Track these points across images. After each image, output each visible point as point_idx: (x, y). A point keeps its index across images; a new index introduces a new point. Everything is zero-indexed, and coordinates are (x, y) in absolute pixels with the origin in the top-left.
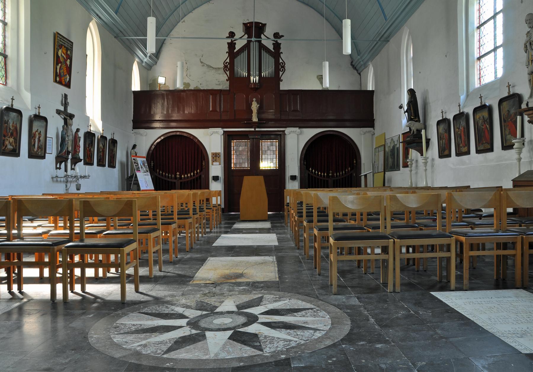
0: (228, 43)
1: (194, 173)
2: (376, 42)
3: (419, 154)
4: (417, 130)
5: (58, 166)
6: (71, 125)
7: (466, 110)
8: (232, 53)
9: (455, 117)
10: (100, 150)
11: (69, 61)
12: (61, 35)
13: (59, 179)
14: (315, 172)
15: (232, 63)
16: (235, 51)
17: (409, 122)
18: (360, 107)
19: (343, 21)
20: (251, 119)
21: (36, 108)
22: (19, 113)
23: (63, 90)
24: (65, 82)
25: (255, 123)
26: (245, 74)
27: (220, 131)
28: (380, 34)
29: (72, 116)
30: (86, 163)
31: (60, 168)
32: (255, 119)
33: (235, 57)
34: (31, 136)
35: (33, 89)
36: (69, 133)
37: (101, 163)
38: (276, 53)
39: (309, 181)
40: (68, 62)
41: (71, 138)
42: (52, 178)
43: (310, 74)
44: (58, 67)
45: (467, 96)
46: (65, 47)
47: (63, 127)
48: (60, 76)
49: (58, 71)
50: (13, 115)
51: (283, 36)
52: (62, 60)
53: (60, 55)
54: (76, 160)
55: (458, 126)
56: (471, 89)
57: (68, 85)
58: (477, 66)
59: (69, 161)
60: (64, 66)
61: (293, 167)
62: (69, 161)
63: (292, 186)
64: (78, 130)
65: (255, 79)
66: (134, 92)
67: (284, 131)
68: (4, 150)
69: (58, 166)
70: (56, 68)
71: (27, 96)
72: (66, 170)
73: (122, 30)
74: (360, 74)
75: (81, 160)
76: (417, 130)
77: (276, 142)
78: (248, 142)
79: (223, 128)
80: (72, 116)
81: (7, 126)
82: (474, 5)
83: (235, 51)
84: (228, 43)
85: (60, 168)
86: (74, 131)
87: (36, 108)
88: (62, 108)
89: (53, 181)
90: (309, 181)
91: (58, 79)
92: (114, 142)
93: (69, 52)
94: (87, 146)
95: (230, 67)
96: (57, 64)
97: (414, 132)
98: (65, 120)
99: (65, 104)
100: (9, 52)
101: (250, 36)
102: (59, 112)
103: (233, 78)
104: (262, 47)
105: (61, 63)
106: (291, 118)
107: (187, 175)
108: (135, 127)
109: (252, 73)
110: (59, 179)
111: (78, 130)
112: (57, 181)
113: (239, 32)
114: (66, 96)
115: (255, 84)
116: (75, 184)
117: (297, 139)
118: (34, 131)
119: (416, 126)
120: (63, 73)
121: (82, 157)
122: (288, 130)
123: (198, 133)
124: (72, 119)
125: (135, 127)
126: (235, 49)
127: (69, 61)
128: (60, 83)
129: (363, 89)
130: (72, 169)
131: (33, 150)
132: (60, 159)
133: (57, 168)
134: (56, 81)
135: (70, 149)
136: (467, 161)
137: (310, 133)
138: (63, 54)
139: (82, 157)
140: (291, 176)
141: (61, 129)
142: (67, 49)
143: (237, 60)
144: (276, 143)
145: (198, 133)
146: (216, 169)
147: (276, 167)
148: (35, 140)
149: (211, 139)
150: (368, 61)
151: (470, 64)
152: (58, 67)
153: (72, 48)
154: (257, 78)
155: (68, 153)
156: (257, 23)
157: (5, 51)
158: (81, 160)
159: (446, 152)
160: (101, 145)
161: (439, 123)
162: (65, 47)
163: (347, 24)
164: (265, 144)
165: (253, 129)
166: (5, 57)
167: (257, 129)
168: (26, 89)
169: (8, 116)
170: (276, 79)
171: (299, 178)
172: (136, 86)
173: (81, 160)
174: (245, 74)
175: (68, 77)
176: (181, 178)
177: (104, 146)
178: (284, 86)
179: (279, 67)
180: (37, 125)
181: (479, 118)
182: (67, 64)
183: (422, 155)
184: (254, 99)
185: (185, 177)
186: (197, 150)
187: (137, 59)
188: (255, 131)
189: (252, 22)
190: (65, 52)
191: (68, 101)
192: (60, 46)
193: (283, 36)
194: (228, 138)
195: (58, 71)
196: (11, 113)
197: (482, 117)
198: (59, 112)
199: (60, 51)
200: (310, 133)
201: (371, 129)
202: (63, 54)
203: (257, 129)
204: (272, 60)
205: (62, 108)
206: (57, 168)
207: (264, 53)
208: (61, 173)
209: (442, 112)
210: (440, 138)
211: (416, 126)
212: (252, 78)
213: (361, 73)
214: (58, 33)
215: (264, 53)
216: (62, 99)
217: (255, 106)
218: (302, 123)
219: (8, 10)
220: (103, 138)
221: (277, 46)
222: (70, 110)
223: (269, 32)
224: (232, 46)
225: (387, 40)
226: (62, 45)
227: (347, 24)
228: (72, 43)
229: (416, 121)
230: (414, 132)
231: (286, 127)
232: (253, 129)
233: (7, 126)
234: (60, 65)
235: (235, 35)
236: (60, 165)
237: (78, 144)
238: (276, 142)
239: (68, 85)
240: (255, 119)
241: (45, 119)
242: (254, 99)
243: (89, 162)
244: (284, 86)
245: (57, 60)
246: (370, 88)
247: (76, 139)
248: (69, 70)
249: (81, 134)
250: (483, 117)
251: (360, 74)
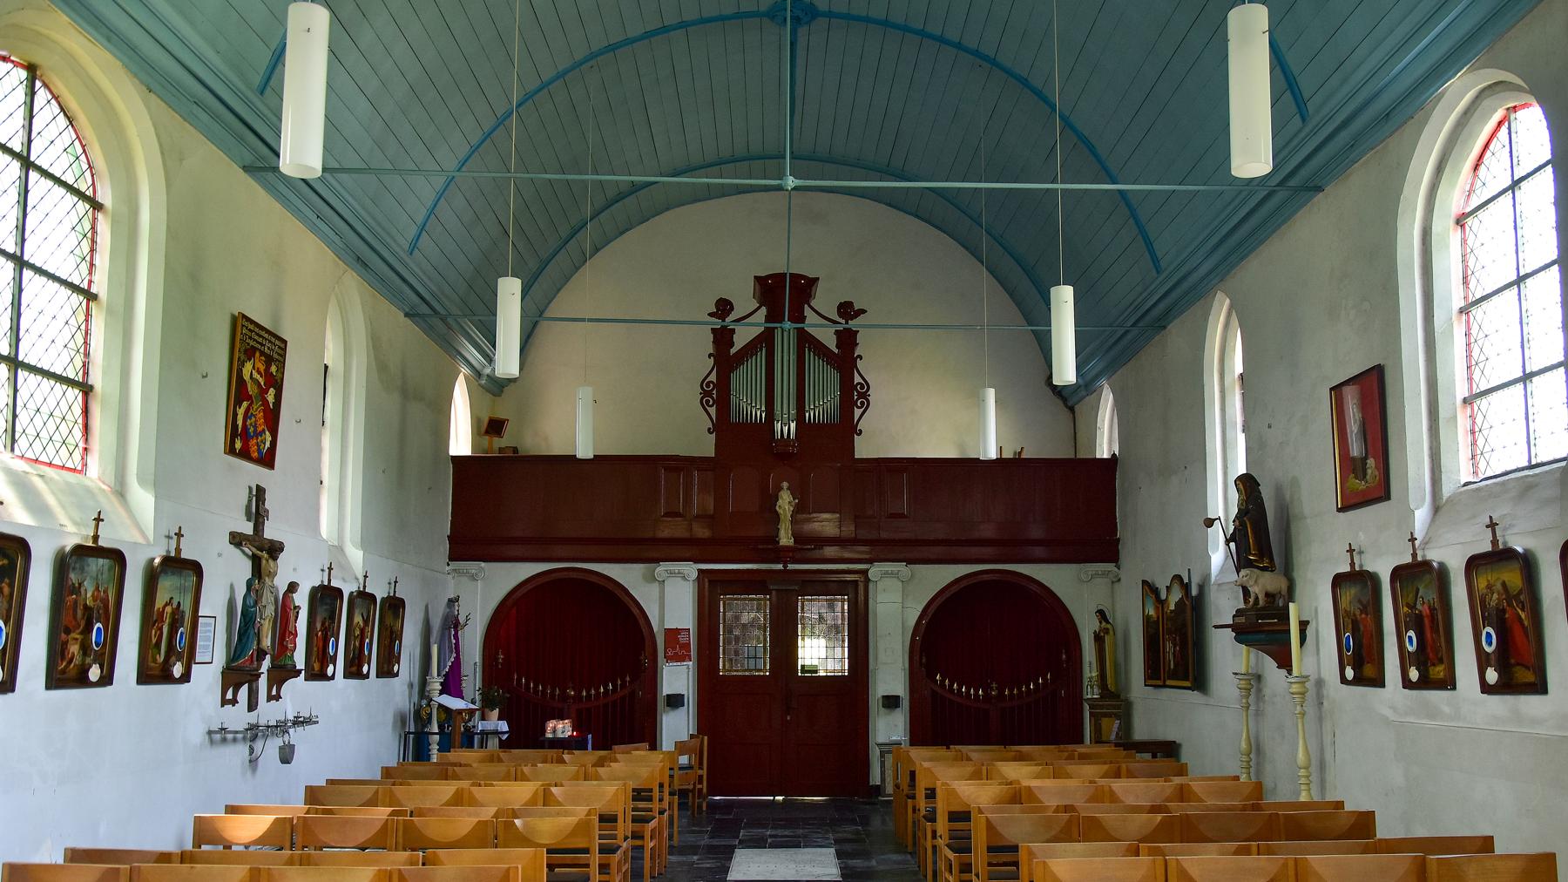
0: (713, 330)
1: (615, 686)
2: (1121, 331)
3: (1270, 664)
4: (1267, 595)
5: (229, 696)
6: (272, 575)
7: (1434, 555)
8: (725, 357)
9: (1398, 573)
10: (354, 630)
11: (272, 391)
12: (252, 322)
13: (230, 736)
14: (951, 685)
15: (723, 385)
16: (733, 351)
17: (1243, 572)
18: (1074, 503)
19: (1053, 290)
20: (774, 539)
21: (169, 537)
22: (117, 557)
23: (252, 473)
24: (259, 450)
25: (787, 549)
26: (759, 413)
27: (691, 570)
28: (1137, 308)
29: (275, 549)
30: (312, 676)
31: (234, 702)
32: (786, 539)
33: (732, 369)
34: (149, 618)
35: (163, 483)
36: (267, 598)
37: (354, 670)
38: (844, 358)
39: (936, 724)
40: (270, 398)
41: (270, 611)
42: (210, 733)
43: (938, 411)
44: (241, 412)
45: (1436, 509)
46: (262, 353)
47: (249, 584)
48: (246, 436)
49: (240, 422)
50: (97, 565)
51: (863, 311)
52: (252, 389)
53: (246, 377)
54: (282, 673)
55: (1410, 599)
56: (1447, 490)
57: (268, 460)
58: (1463, 423)
59: (263, 682)
60: (257, 409)
61: (890, 675)
62: (263, 682)
63: (889, 728)
64: (293, 587)
65: (786, 428)
66: (458, 461)
67: (865, 572)
68: (64, 672)
69: (229, 696)
70: (235, 415)
71: (144, 500)
72: (252, 706)
73: (427, 296)
74: (1072, 409)
75: (299, 672)
76: (1267, 595)
77: (843, 601)
78: (766, 601)
79: (696, 561)
80: (275, 549)
81: (76, 602)
82: (1447, 246)
83: (733, 351)
84: (713, 330)
85: (234, 702)
86: (283, 589)
87: (169, 537)
88: (248, 528)
89: (212, 742)
90: (936, 724)
91: (238, 445)
92: (395, 605)
93: (273, 369)
94: (319, 626)
95: (718, 393)
96: (238, 403)
97: (1257, 598)
98: (256, 562)
99: (258, 514)
100: (96, 379)
101: (774, 316)
102: (237, 539)
103: (725, 426)
104: (806, 341)
105: (249, 398)
106: (884, 535)
107: (597, 689)
108: (454, 556)
109: (778, 411)
110: (230, 736)
111: (293, 587)
112: (224, 740)
113: (745, 300)
114: (260, 493)
115: (785, 441)
116: (279, 742)
117: (901, 597)
118: (159, 604)
119: (1263, 583)
120: (255, 427)
121: (300, 665)
122: (875, 570)
123: (626, 575)
124: (275, 559)
125: (454, 556)
126: (732, 345)
127: (272, 391)
128: (244, 454)
129: (1082, 455)
130: (270, 698)
131: (155, 661)
132: (236, 676)
133: (224, 702)
134: (231, 450)
135: (267, 642)
136: (1446, 709)
137: (942, 575)
138: (256, 375)
139: (300, 665)
140: (886, 698)
141: (241, 591)
142: (269, 360)
143: (738, 378)
144: (842, 606)
145: (626, 575)
146: (677, 678)
147: (843, 670)
148: (161, 629)
149: (668, 597)
150: (1097, 377)
151: (1443, 413)
152: (241, 412)
153: (284, 356)
154: (793, 425)
155: (261, 654)
156: (796, 278)
157: (86, 373)
158: (297, 673)
159: (1369, 670)
160: (358, 619)
161: (1339, 581)
162: (262, 353)
163: (1064, 298)
164: (812, 608)
165: (780, 567)
166: (86, 390)
167: (791, 567)
168: (142, 481)
169: (82, 570)
170: (845, 428)
171: (906, 704)
172: (461, 443)
173: (299, 672)
174: (759, 413)
175: (269, 438)
176: (578, 698)
177: (366, 622)
178: (865, 449)
179: (853, 395)
180: (167, 589)
181: (1489, 587)
182: (265, 402)
183: (1285, 662)
184: (785, 485)
185: (589, 695)
186: (623, 621)
187: (464, 370)
188: (785, 571)
189: (782, 276)
190: (262, 368)
191: (267, 506)
192: (250, 353)
193: (863, 311)
194: (711, 591)
195: (240, 422)
196: (91, 560)
197: (1499, 586)
198: (237, 539)
199: (248, 367)
200: (942, 575)
201: (1110, 567)
202: (256, 375)
203: (791, 567)
204: (833, 376)
205: (248, 528)
206: (224, 702)
207: (810, 357)
208: (237, 717)
209: (1351, 551)
210: (1342, 620)
211: (1263, 583)
212: (778, 426)
213: (1077, 408)
214: (244, 316)
215: (810, 357)
216: (250, 501)
217: (785, 503)
218: (913, 551)
219: (103, 260)
220: (364, 597)
221: (848, 339)
222: (271, 532)
223: (825, 301)
224: (723, 338)
225: (1161, 324)
226: (254, 349)
227: (1064, 298)
228: (285, 342)
229: (1264, 569)
230: (1257, 598)
231: (871, 561)
232: (780, 567)
233: (76, 602)
234: (245, 404)
235: (732, 309)
236: (235, 694)
237: (291, 628)
238: (843, 601)
239: (268, 460)
240: (786, 539)
241: (196, 568)
242: (785, 485)
243: (317, 673)
244: (865, 449)
245: (239, 392)
246: (1105, 446)
247: (285, 612)
248: (272, 418)
249: (301, 599)
250: (1504, 584)
251: (1072, 409)
